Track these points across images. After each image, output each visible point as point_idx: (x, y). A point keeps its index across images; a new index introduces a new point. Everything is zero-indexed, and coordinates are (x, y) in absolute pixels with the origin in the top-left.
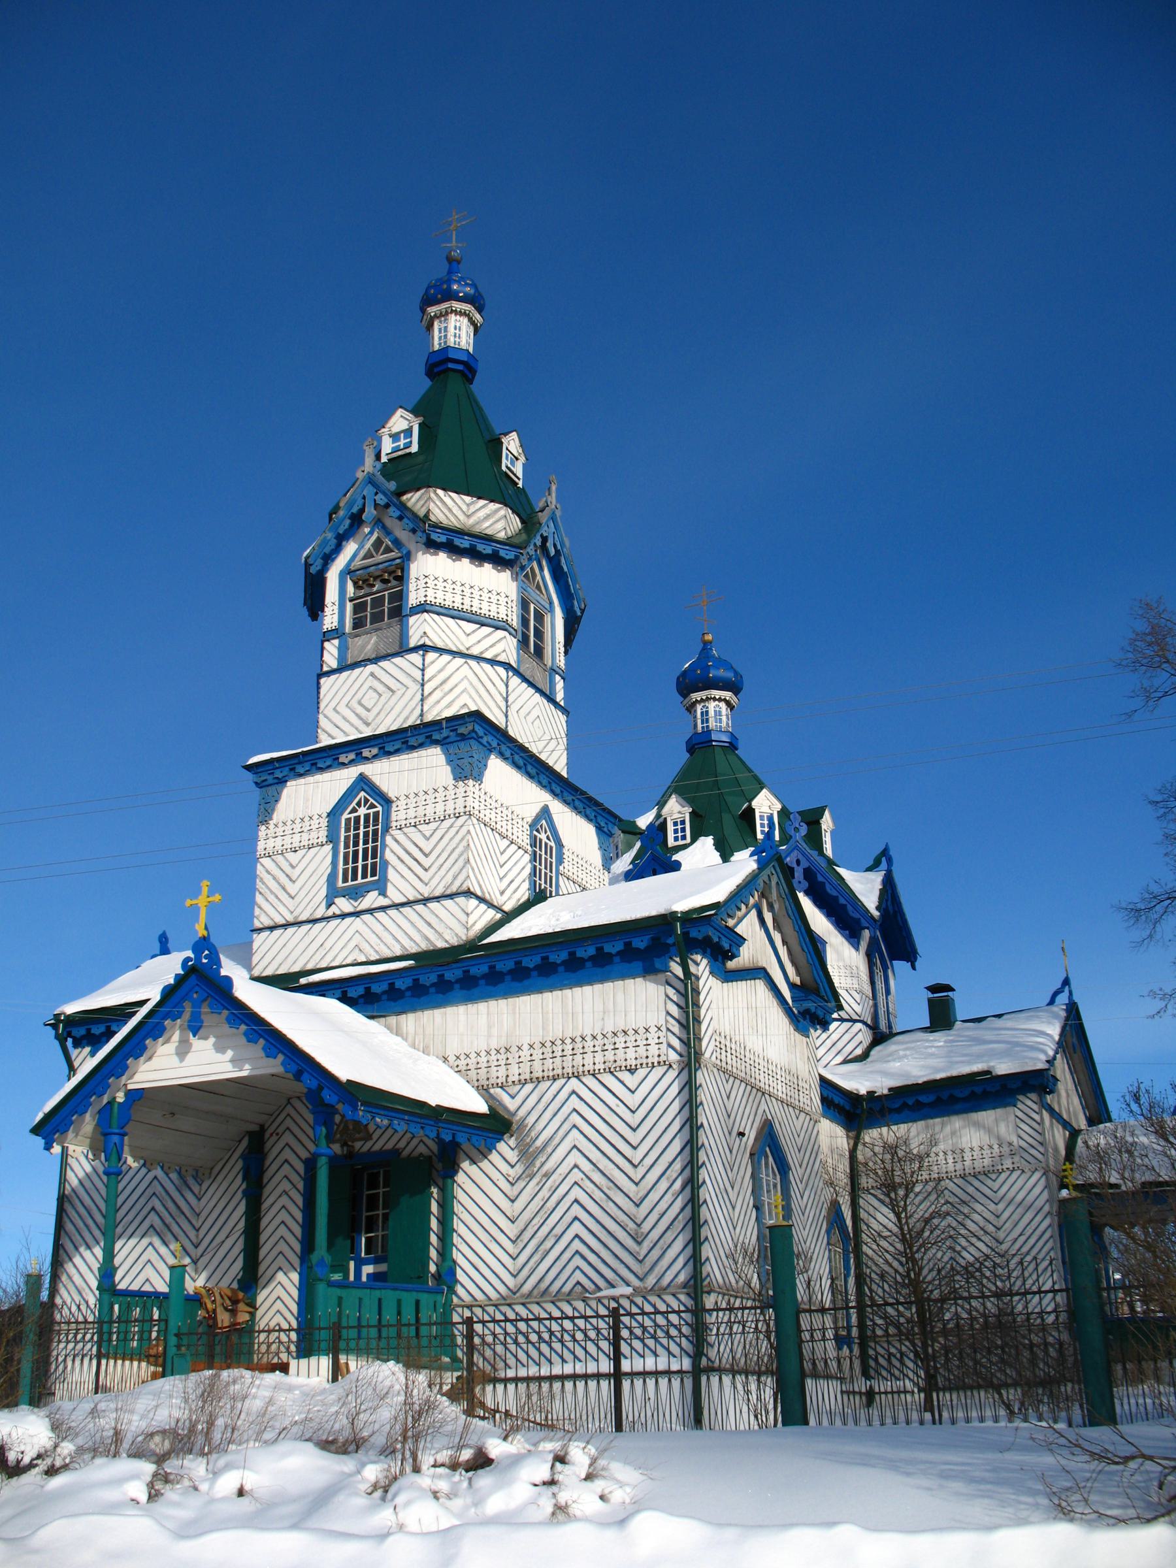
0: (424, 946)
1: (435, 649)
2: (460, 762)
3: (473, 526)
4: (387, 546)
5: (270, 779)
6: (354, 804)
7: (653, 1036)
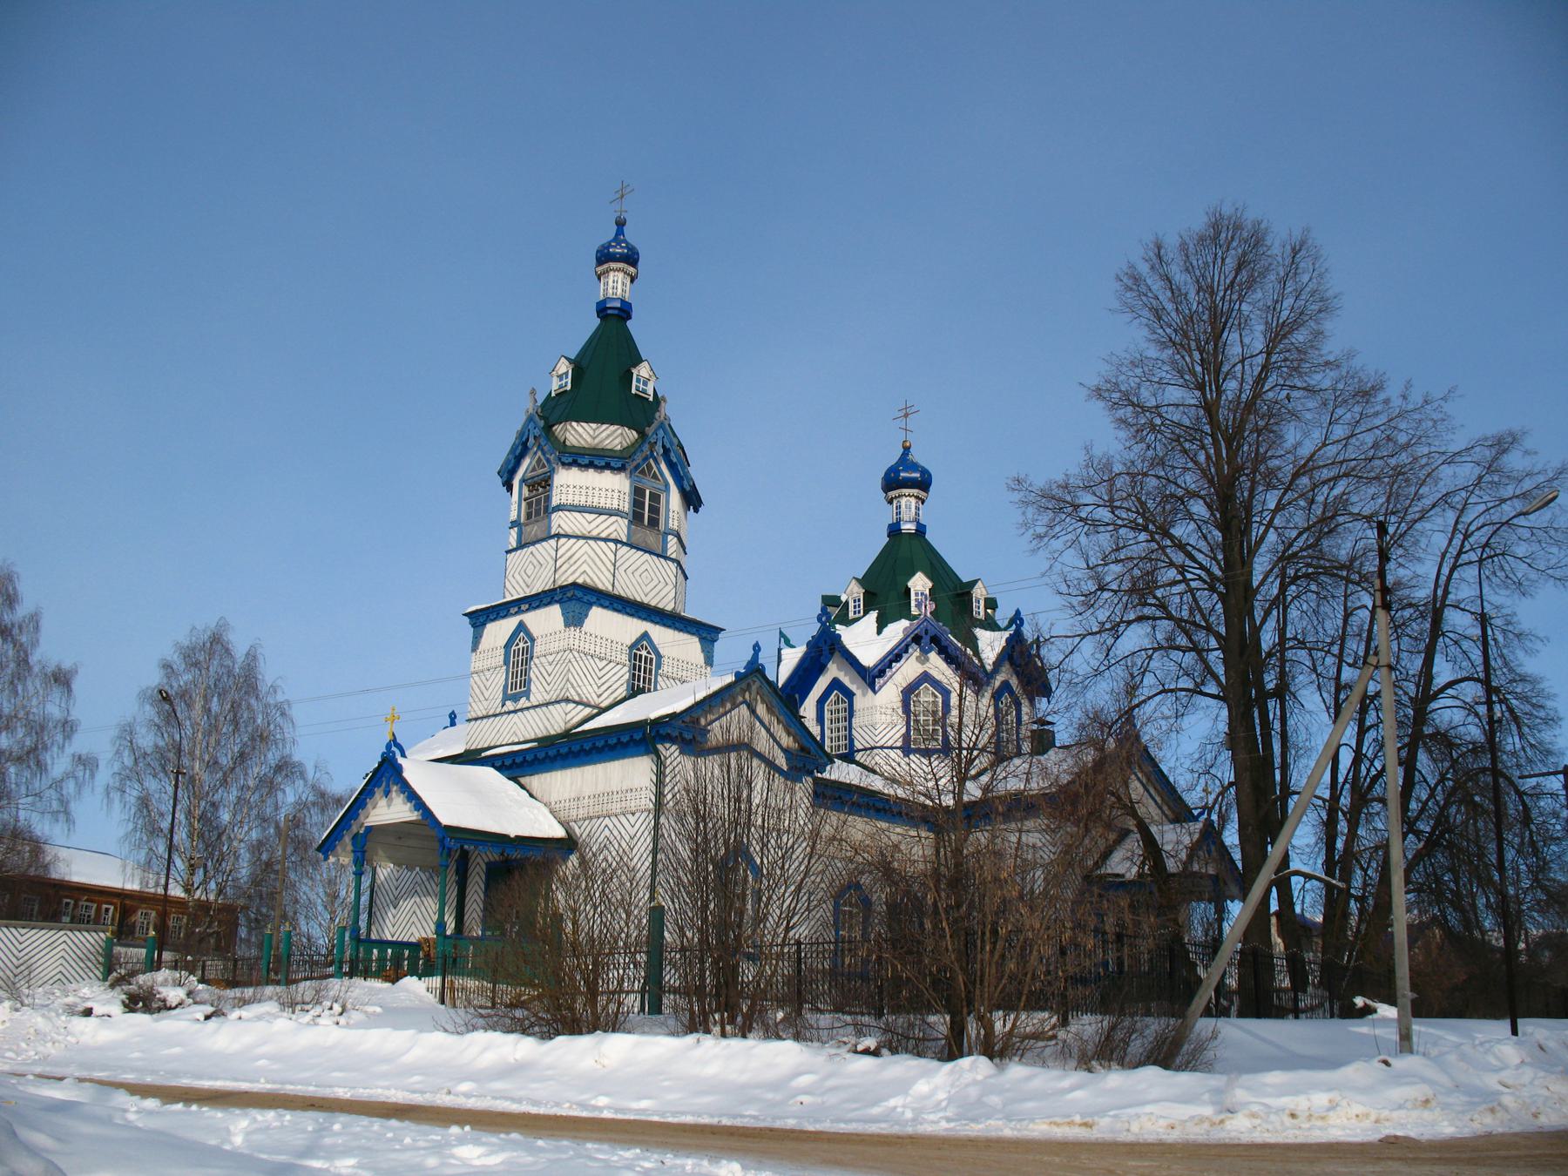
1: (568, 536)
3: (597, 444)
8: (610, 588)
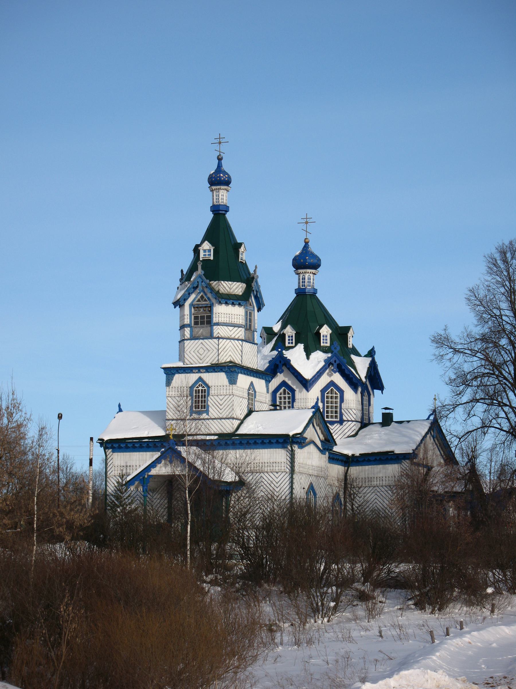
0: (220, 432)
2: (231, 379)
4: (205, 299)
5: (170, 373)
6: (198, 385)
7: (283, 465)
8: (241, 363)
